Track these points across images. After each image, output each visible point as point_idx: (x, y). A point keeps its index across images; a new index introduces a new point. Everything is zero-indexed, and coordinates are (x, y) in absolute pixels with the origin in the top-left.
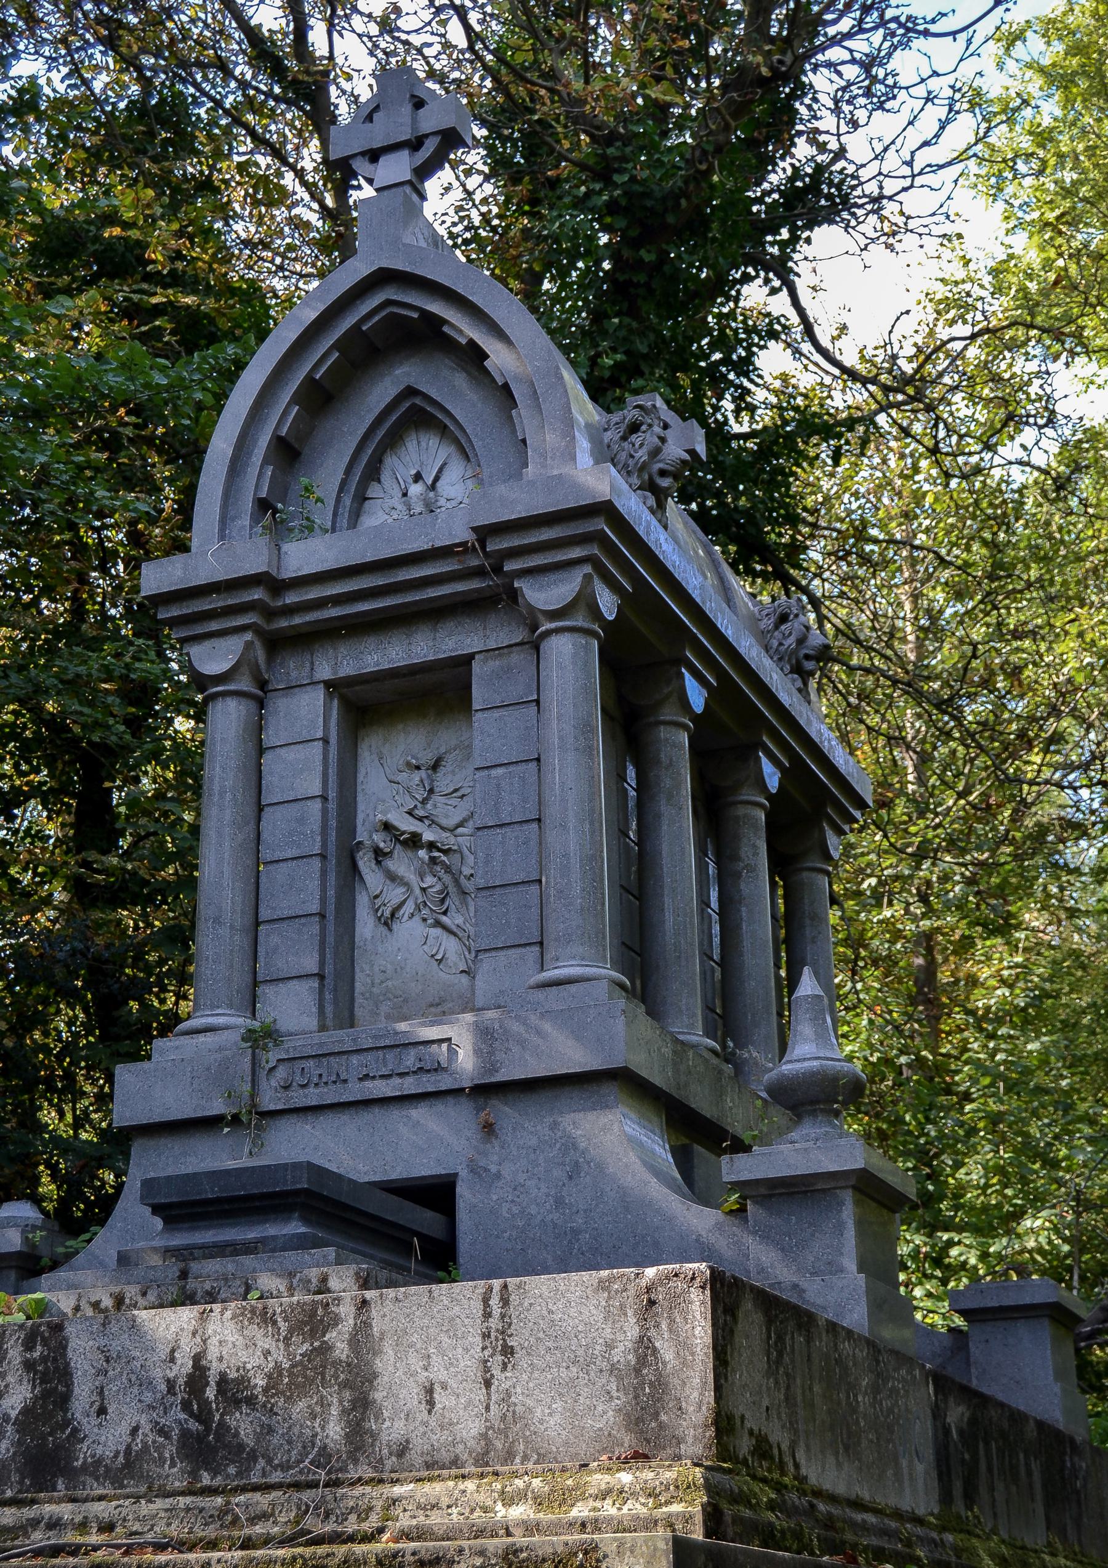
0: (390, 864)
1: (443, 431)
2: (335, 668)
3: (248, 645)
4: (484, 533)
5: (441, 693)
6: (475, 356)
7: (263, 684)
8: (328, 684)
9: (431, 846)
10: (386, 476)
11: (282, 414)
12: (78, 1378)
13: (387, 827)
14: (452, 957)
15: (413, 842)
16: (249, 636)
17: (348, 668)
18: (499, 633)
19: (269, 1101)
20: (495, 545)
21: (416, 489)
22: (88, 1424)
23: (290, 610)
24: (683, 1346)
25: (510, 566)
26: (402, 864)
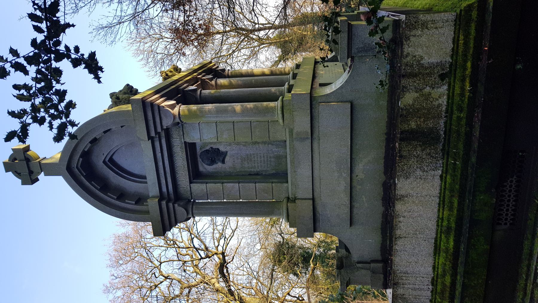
3: (179, 205)
4: (150, 138)
6: (94, 141)
8: (191, 182)
16: (176, 205)
19: (311, 196)
20: (153, 134)
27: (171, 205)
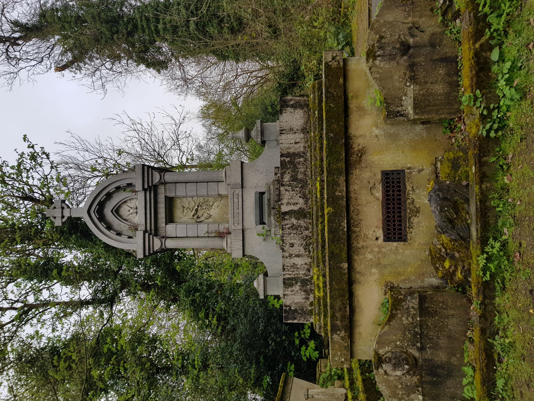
0: (200, 216)
1: (120, 206)
2: (163, 223)
5: (170, 202)
7: (163, 237)
8: (166, 224)
9: (198, 207)
10: (127, 218)
11: (112, 234)
12: (291, 209)
13: (193, 216)
14: (218, 204)
15: (197, 210)
17: (164, 220)
18: (161, 190)
19: (240, 227)
20: (146, 187)
21: (131, 211)
22: (299, 206)
23: (151, 230)
24: (291, 100)
25: (150, 185)
26: (200, 213)
27: (151, 236)
